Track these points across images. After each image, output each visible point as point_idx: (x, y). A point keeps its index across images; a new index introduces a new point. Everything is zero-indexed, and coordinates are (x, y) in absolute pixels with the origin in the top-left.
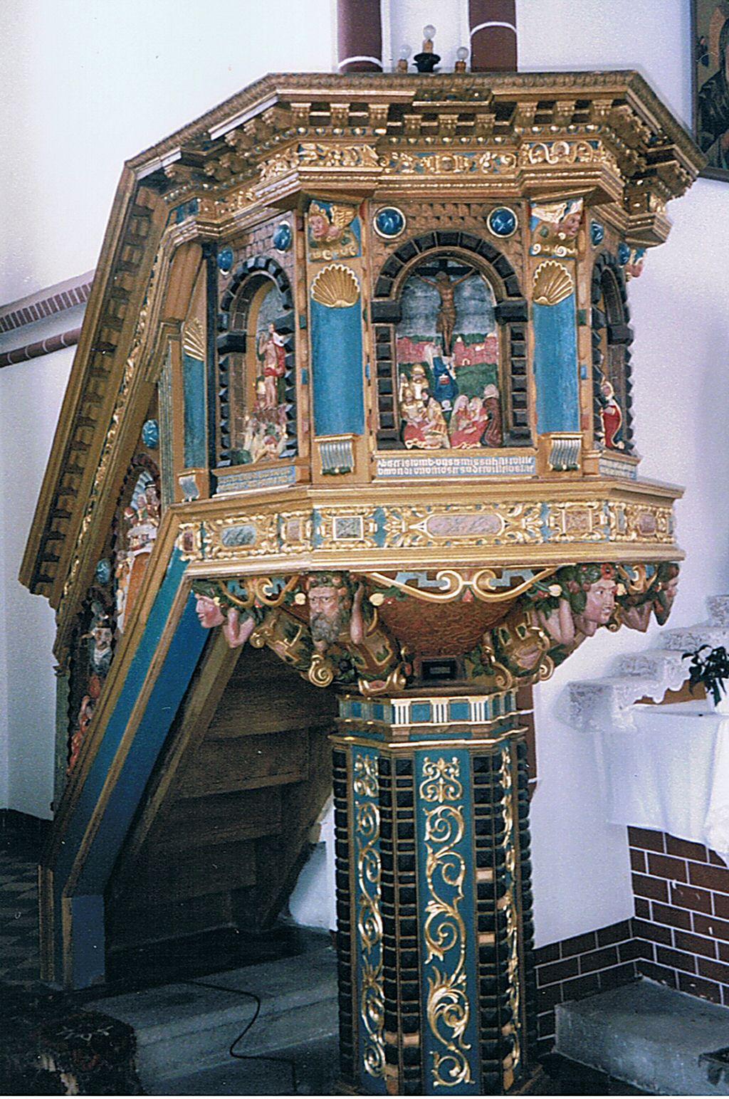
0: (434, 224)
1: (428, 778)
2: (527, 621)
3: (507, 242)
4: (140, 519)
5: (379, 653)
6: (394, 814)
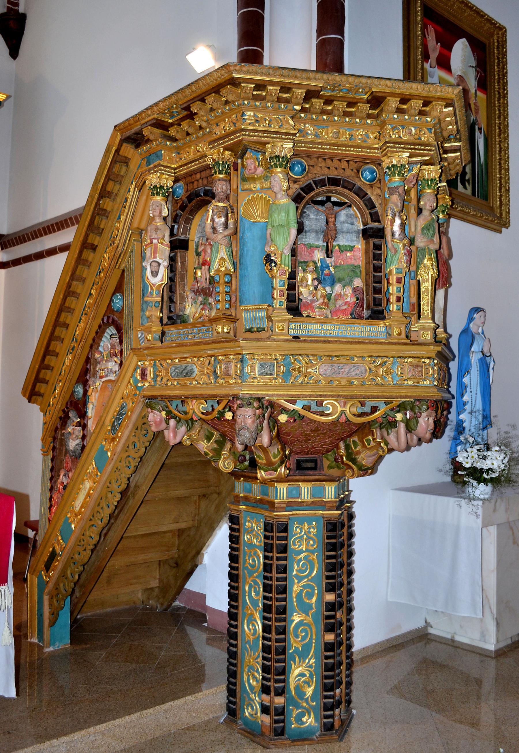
0: (326, 171)
1: (296, 534)
2: (373, 436)
3: (372, 187)
4: (105, 359)
5: (274, 453)
6: (275, 558)
